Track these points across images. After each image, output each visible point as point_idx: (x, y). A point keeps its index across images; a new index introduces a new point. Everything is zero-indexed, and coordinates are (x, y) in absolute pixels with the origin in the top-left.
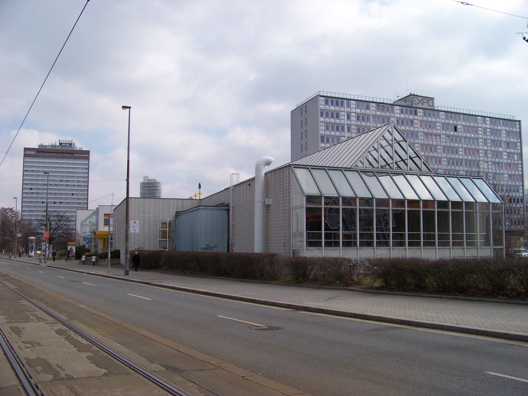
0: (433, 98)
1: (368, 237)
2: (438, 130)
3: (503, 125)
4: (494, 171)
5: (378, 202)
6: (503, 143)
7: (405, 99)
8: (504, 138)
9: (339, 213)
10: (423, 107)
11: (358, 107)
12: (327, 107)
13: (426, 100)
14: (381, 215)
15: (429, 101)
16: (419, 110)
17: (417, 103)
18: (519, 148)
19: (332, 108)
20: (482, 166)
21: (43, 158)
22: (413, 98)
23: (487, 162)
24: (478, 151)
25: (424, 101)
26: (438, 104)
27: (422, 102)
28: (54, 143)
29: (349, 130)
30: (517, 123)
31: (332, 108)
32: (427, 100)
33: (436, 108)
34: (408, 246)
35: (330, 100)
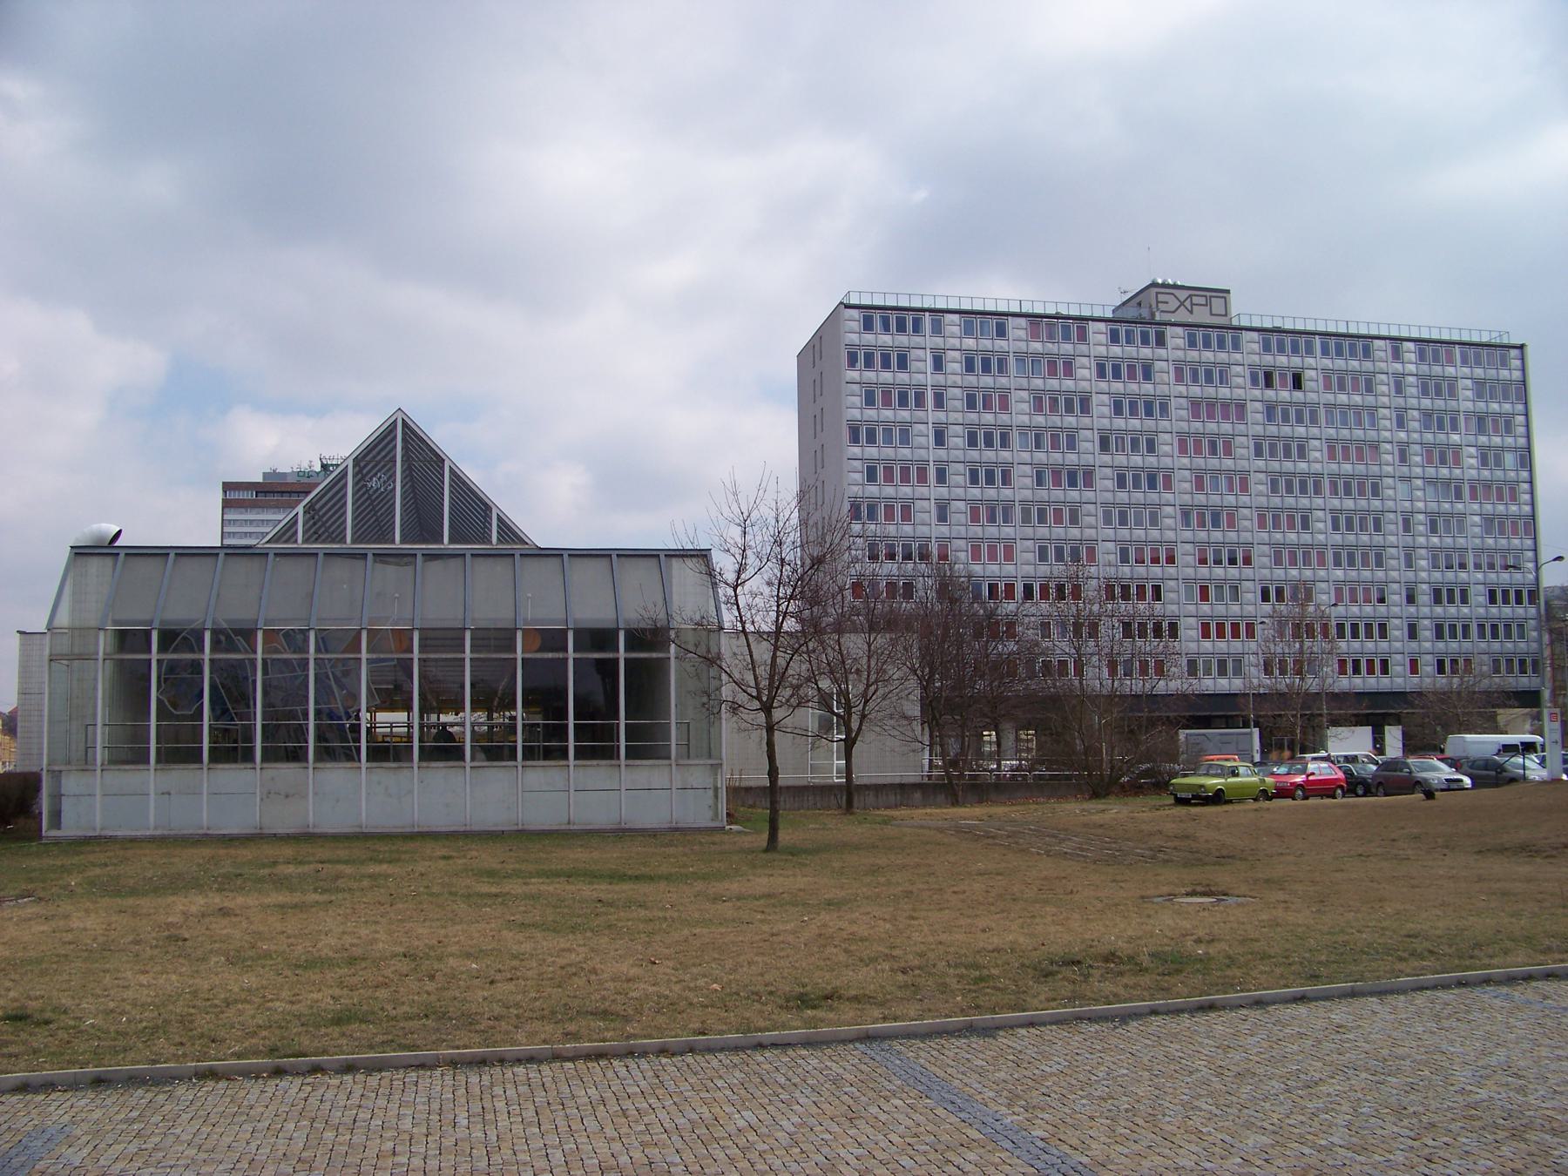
0: (1228, 292)
1: (290, 736)
2: (1240, 387)
3: (1465, 362)
4: (1434, 505)
5: (323, 638)
6: (1462, 417)
7: (1137, 299)
8: (1466, 400)
9: (201, 672)
10: (1190, 319)
11: (968, 331)
12: (869, 338)
13: (1204, 299)
14: (333, 673)
16: (1169, 331)
17: (1173, 309)
18: (1521, 430)
19: (886, 339)
20: (1391, 492)
21: (276, 510)
22: (1157, 293)
23: (1408, 479)
24: (1377, 448)
25: (1195, 300)
26: (1243, 310)
27: (1188, 303)
28: (305, 466)
29: (939, 402)
30: (1514, 353)
31: (886, 339)
32: (1206, 296)
33: (1235, 322)
34: (576, 758)
35: (877, 318)
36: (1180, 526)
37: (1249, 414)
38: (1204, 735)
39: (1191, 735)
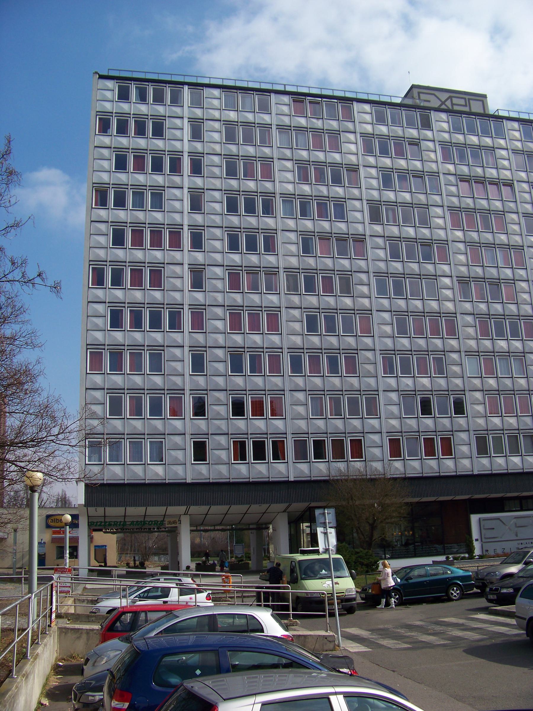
0: (485, 96)
15: (471, 102)
16: (434, 116)
20: (457, 369)
32: (465, 99)
36: (458, 298)
37: (376, 327)
38: (498, 519)
39: (485, 519)
